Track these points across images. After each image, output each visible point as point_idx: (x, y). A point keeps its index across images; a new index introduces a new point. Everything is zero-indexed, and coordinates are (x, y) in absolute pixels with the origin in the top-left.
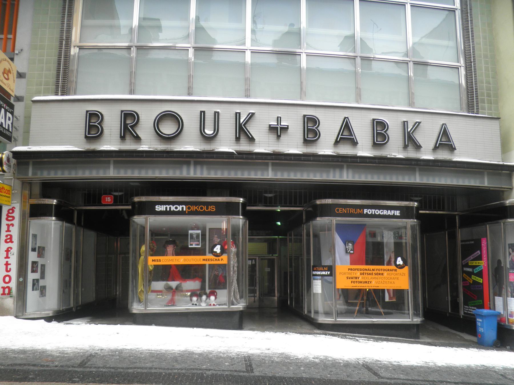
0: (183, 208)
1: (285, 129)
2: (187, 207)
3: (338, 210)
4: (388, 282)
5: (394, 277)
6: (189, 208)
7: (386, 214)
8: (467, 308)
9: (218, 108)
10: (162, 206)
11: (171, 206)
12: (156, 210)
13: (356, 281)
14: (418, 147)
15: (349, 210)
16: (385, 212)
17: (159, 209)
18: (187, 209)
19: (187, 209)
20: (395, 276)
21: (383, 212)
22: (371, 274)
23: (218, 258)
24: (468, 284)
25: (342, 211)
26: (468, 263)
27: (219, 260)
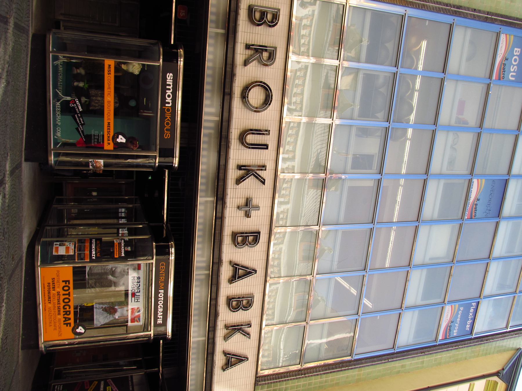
0: (169, 103)
1: (247, 215)
2: (170, 108)
3: (163, 265)
4: (51, 319)
5: (57, 326)
6: (168, 110)
7: (159, 311)
8: (60, 388)
9: (272, 146)
10: (172, 81)
11: (171, 91)
12: (168, 74)
13: (50, 288)
14: (226, 338)
15: (163, 276)
16: (160, 310)
17: (171, 76)
18: (167, 108)
19: (167, 108)
20: (57, 327)
21: (161, 308)
22: (59, 303)
23: (111, 139)
24: (86, 388)
25: (161, 269)
26: (109, 386)
27: (109, 140)
